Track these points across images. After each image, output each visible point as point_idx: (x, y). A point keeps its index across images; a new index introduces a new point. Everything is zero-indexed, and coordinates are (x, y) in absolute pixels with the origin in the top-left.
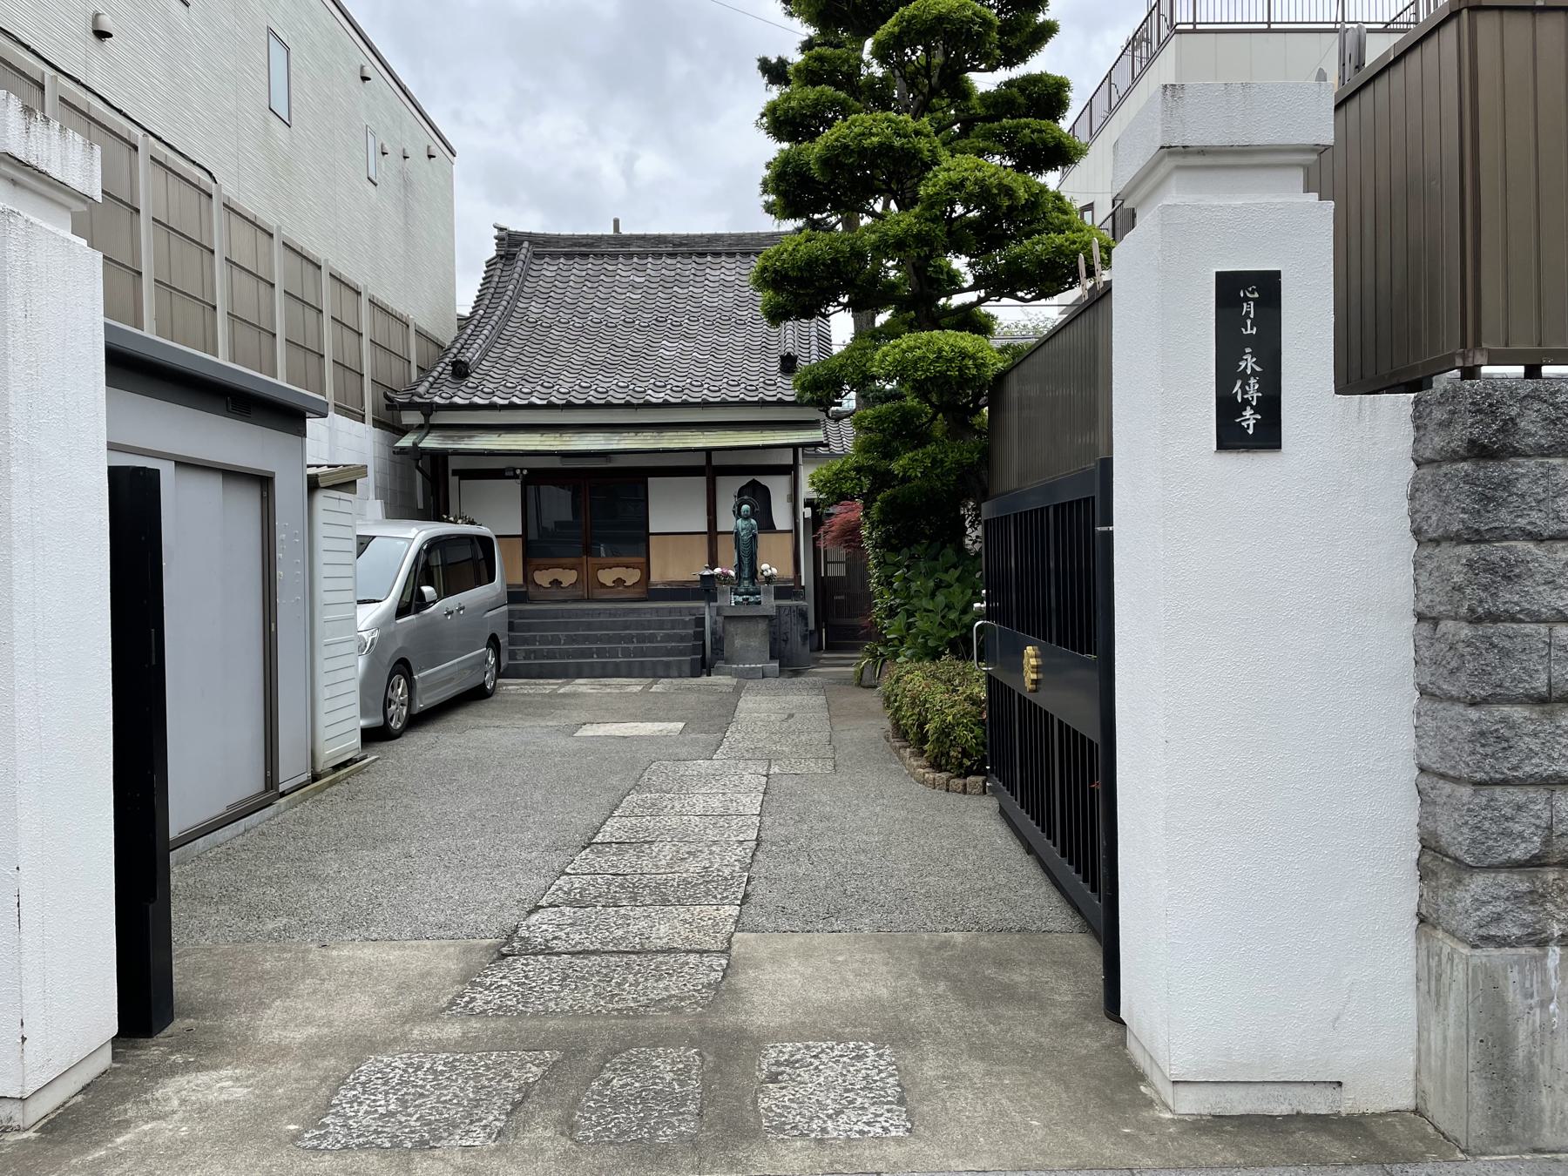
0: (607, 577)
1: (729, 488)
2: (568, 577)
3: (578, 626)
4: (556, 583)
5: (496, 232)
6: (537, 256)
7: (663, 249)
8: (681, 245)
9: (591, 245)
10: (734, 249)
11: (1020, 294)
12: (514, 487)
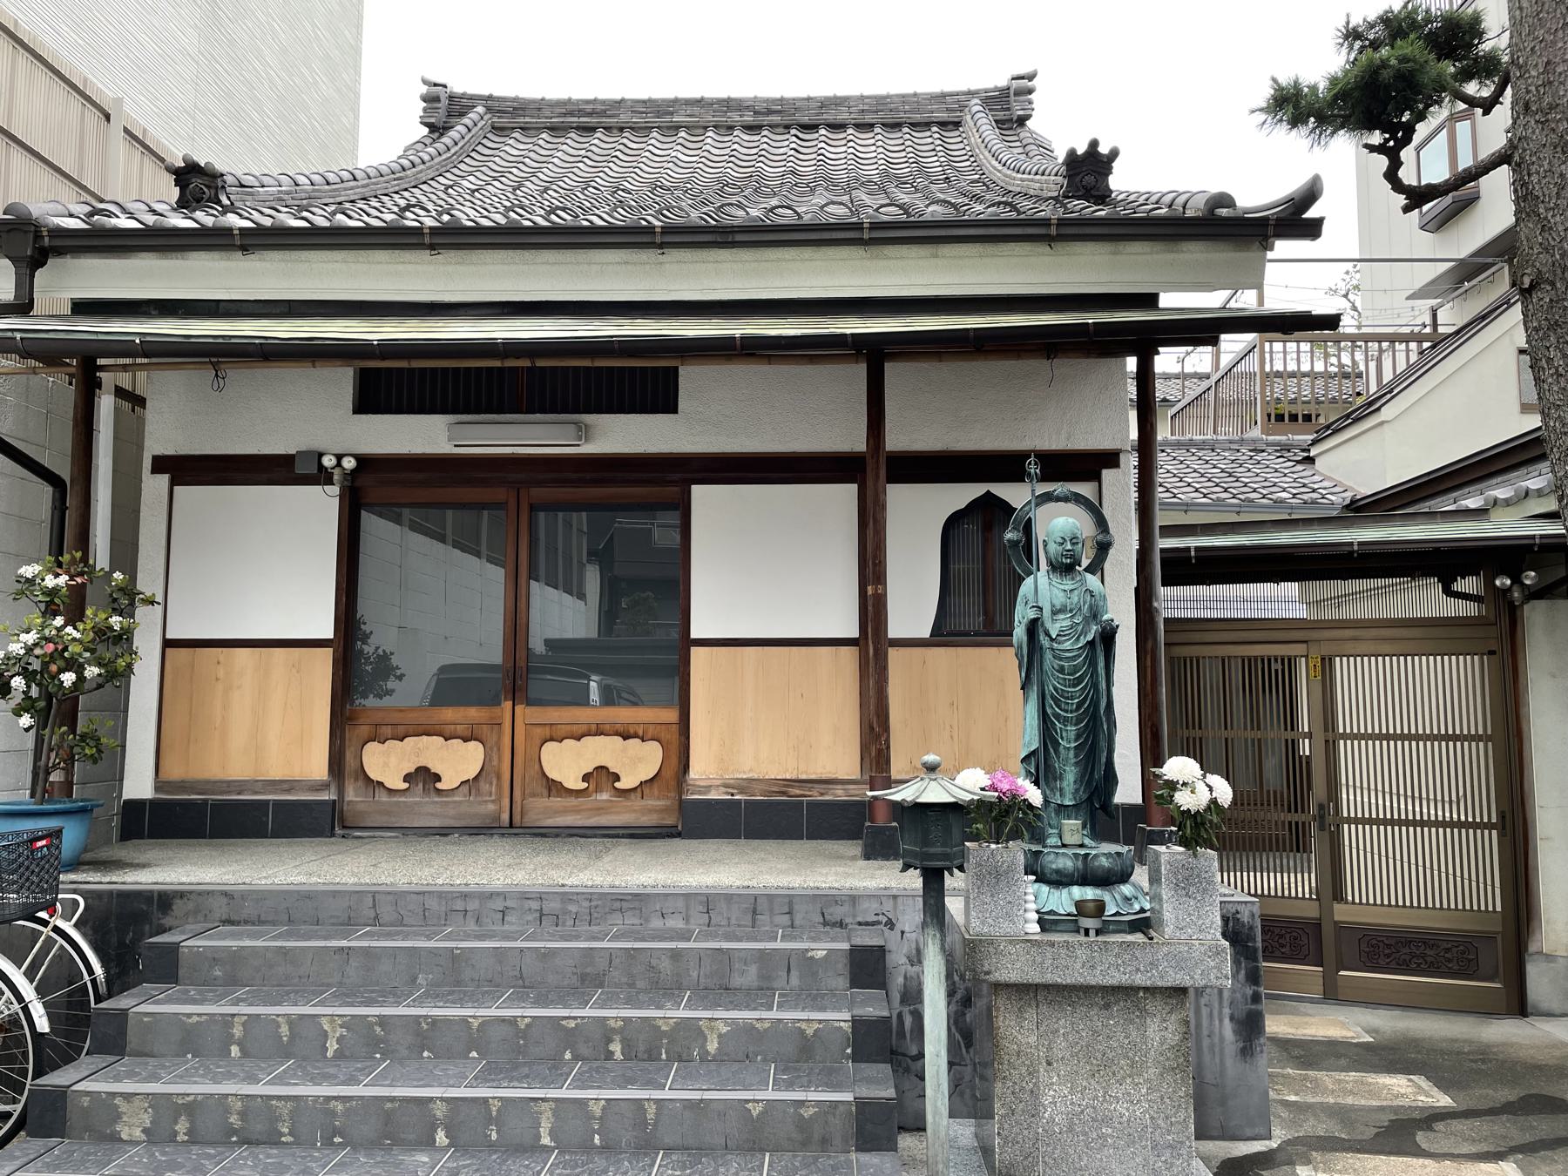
0: (567, 762)
1: (919, 517)
2: (457, 762)
3: (406, 974)
4: (424, 777)
5: (424, 89)
6: (498, 130)
7: (735, 117)
8: (770, 112)
9: (603, 114)
10: (868, 118)
11: (767, 1025)
12: (319, 508)
